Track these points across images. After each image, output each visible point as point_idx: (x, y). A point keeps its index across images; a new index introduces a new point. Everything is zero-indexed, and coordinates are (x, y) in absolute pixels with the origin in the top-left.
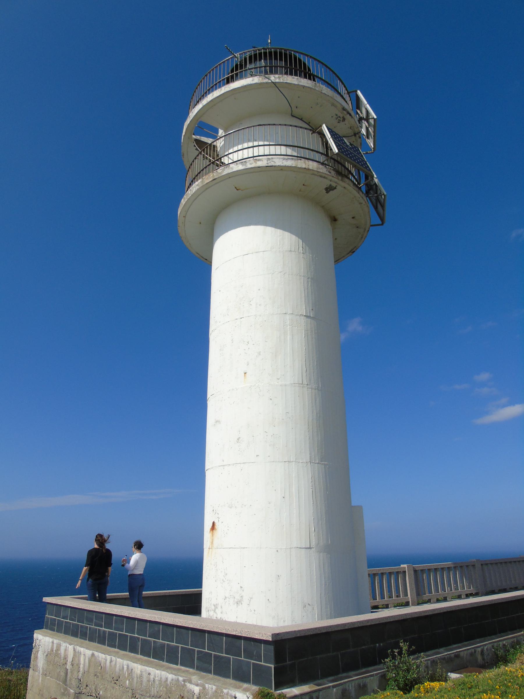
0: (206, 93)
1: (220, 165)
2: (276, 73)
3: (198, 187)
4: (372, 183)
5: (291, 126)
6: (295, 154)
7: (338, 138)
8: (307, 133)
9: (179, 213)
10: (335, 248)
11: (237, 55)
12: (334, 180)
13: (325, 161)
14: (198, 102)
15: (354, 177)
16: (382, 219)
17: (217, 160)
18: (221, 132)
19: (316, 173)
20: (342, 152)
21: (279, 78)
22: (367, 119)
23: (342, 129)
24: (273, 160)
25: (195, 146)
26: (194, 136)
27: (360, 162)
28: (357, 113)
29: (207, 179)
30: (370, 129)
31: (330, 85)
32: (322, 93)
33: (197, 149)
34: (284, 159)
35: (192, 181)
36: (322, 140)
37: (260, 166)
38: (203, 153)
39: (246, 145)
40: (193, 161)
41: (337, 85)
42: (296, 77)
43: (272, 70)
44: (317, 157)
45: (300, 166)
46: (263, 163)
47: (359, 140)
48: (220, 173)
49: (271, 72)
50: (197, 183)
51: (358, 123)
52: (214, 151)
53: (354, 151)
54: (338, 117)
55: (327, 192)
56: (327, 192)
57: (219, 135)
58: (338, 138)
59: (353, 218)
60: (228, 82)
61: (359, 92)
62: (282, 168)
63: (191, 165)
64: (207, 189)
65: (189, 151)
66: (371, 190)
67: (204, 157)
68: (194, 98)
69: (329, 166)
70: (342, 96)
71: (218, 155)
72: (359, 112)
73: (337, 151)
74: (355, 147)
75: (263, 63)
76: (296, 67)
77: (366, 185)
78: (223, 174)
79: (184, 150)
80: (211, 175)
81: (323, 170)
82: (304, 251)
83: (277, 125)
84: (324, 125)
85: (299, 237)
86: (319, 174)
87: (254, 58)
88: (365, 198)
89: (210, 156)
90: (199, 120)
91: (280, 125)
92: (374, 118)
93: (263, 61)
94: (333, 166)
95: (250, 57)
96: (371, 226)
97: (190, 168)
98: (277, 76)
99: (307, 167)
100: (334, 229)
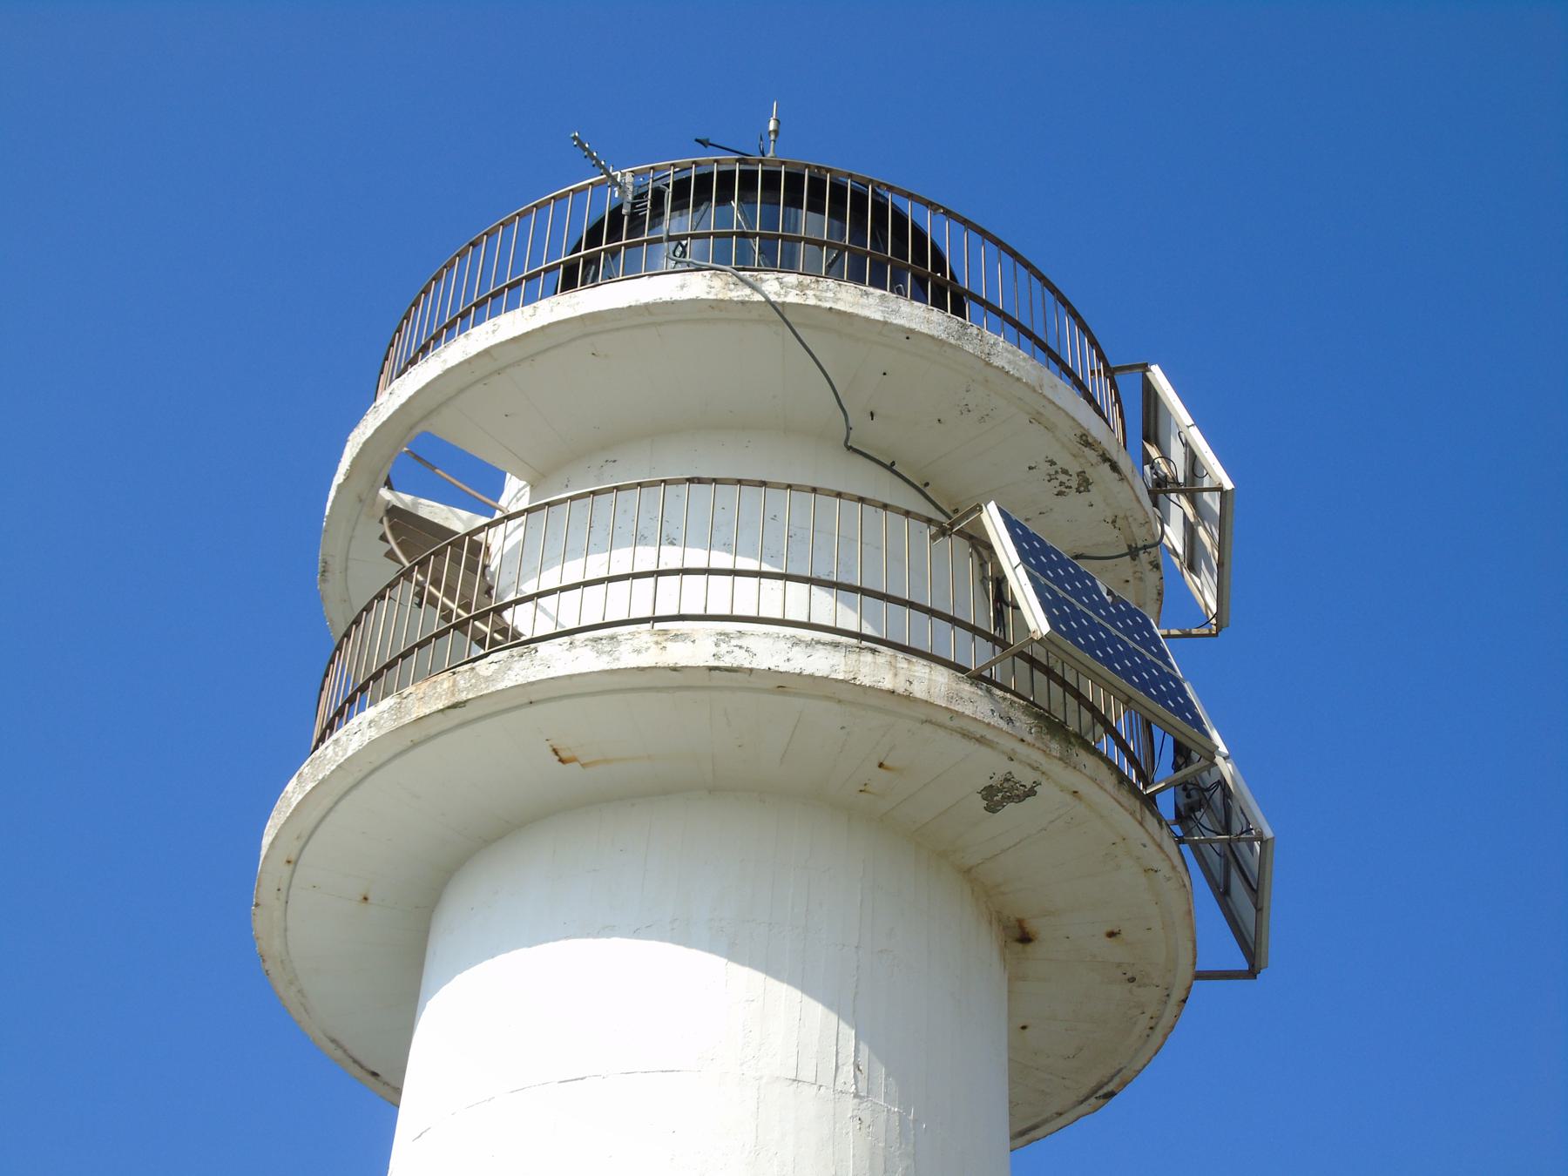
0: (464, 315)
1: (494, 643)
2: (789, 266)
3: (373, 733)
4: (1209, 780)
5: (839, 495)
6: (850, 621)
7: (1052, 565)
8: (912, 538)
9: (266, 841)
10: (1021, 1070)
11: (625, 176)
12: (1025, 752)
13: (989, 666)
14: (424, 350)
15: (1123, 746)
16: (1251, 949)
17: (482, 617)
18: (515, 493)
19: (944, 718)
20: (1071, 635)
21: (801, 287)
22: (1192, 490)
23: (1072, 525)
24: (744, 642)
25: (383, 538)
26: (385, 494)
27: (1154, 682)
28: (1147, 459)
29: (424, 697)
30: (1201, 530)
31: (1030, 335)
32: (989, 364)
33: (390, 555)
34: (797, 642)
35: (351, 700)
36: (983, 565)
37: (682, 663)
38: (417, 576)
39: (622, 561)
40: (368, 609)
41: (1060, 338)
42: (879, 292)
43: (777, 253)
44: (953, 643)
45: (867, 682)
46: (697, 649)
47: (1152, 577)
48: (487, 679)
49: (770, 264)
50: (370, 713)
51: (1147, 501)
52: (472, 568)
53: (1128, 631)
54: (1056, 472)
55: (992, 808)
56: (992, 808)
57: (503, 502)
58: (1052, 565)
59: (1111, 935)
60: (569, 283)
61: (1157, 375)
62: (783, 684)
63: (357, 622)
64: (415, 745)
65: (359, 561)
66: (1200, 805)
67: (420, 594)
68: (407, 329)
69: (1006, 689)
70: (1080, 386)
71: (488, 591)
72: (1154, 452)
73: (1045, 628)
74: (1133, 613)
75: (737, 215)
76: (885, 243)
77: (1185, 787)
78: (500, 686)
79: (331, 547)
80: (444, 681)
81: (976, 704)
82: (863, 1085)
83: (777, 486)
84: (992, 506)
85: (841, 1016)
86: (957, 723)
87: (694, 191)
88: (1170, 846)
89: (450, 593)
90: (418, 430)
91: (789, 486)
92: (1220, 489)
93: (734, 204)
94: (1025, 691)
95: (681, 187)
96: (1200, 976)
97: (347, 635)
98: (791, 279)
99: (901, 687)
100: (1015, 979)
